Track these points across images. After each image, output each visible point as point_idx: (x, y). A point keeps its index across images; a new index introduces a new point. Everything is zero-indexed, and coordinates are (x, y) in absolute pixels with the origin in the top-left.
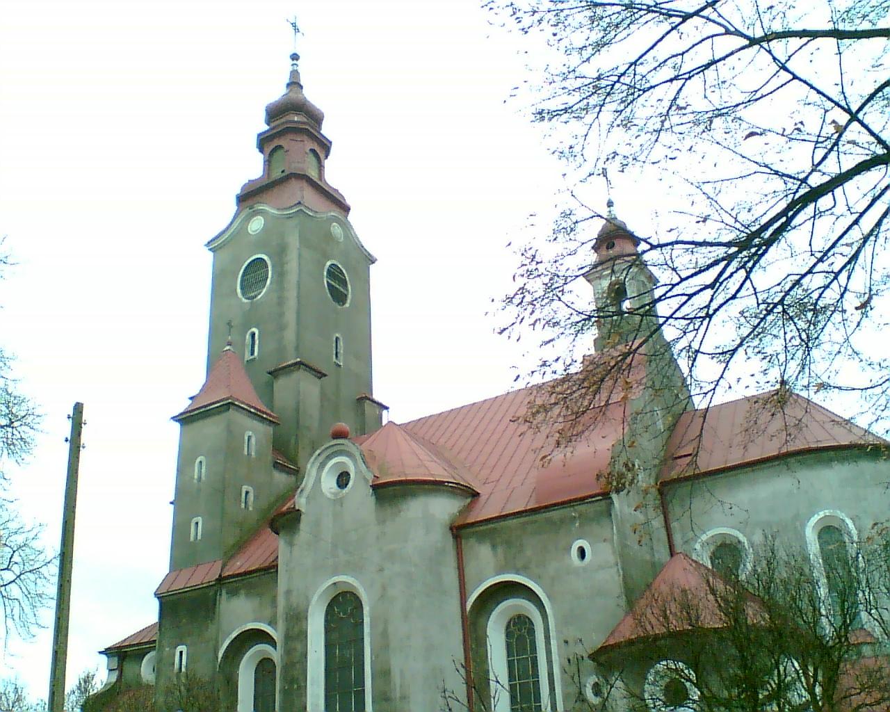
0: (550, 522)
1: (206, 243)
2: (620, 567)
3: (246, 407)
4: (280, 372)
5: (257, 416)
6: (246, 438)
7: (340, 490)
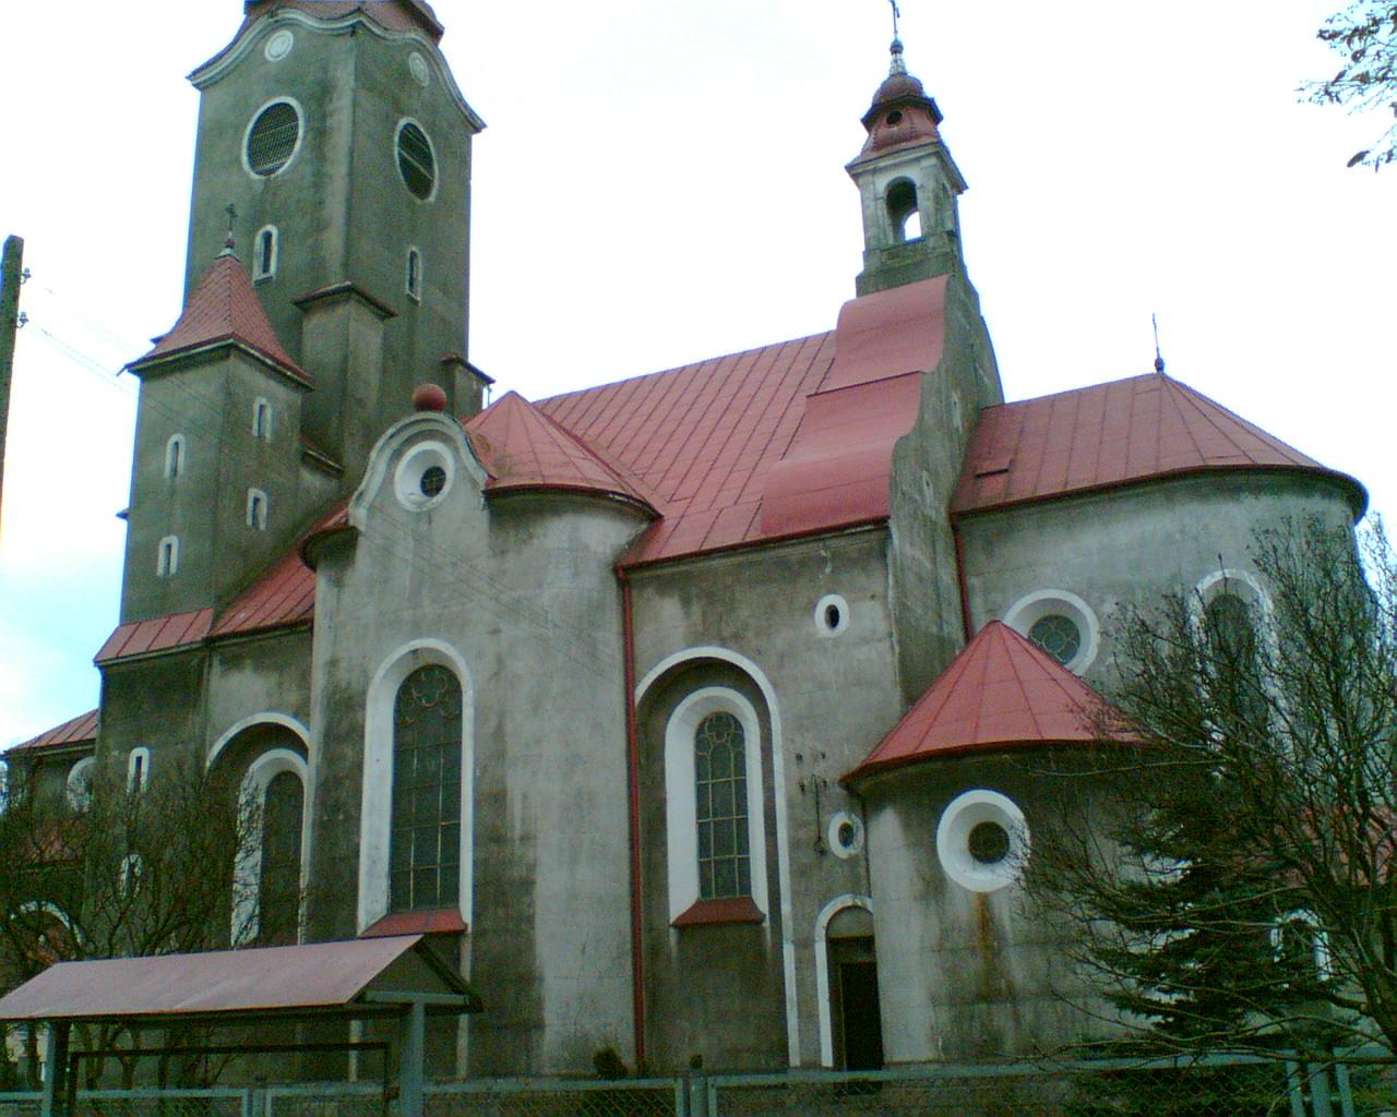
0: (783, 564)
1: (189, 73)
2: (894, 639)
3: (257, 354)
4: (316, 302)
5: (276, 372)
6: (256, 408)
7: (426, 498)
